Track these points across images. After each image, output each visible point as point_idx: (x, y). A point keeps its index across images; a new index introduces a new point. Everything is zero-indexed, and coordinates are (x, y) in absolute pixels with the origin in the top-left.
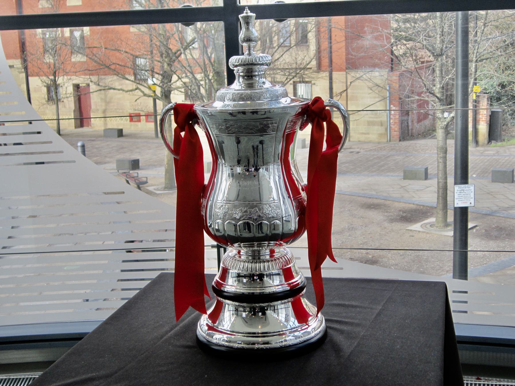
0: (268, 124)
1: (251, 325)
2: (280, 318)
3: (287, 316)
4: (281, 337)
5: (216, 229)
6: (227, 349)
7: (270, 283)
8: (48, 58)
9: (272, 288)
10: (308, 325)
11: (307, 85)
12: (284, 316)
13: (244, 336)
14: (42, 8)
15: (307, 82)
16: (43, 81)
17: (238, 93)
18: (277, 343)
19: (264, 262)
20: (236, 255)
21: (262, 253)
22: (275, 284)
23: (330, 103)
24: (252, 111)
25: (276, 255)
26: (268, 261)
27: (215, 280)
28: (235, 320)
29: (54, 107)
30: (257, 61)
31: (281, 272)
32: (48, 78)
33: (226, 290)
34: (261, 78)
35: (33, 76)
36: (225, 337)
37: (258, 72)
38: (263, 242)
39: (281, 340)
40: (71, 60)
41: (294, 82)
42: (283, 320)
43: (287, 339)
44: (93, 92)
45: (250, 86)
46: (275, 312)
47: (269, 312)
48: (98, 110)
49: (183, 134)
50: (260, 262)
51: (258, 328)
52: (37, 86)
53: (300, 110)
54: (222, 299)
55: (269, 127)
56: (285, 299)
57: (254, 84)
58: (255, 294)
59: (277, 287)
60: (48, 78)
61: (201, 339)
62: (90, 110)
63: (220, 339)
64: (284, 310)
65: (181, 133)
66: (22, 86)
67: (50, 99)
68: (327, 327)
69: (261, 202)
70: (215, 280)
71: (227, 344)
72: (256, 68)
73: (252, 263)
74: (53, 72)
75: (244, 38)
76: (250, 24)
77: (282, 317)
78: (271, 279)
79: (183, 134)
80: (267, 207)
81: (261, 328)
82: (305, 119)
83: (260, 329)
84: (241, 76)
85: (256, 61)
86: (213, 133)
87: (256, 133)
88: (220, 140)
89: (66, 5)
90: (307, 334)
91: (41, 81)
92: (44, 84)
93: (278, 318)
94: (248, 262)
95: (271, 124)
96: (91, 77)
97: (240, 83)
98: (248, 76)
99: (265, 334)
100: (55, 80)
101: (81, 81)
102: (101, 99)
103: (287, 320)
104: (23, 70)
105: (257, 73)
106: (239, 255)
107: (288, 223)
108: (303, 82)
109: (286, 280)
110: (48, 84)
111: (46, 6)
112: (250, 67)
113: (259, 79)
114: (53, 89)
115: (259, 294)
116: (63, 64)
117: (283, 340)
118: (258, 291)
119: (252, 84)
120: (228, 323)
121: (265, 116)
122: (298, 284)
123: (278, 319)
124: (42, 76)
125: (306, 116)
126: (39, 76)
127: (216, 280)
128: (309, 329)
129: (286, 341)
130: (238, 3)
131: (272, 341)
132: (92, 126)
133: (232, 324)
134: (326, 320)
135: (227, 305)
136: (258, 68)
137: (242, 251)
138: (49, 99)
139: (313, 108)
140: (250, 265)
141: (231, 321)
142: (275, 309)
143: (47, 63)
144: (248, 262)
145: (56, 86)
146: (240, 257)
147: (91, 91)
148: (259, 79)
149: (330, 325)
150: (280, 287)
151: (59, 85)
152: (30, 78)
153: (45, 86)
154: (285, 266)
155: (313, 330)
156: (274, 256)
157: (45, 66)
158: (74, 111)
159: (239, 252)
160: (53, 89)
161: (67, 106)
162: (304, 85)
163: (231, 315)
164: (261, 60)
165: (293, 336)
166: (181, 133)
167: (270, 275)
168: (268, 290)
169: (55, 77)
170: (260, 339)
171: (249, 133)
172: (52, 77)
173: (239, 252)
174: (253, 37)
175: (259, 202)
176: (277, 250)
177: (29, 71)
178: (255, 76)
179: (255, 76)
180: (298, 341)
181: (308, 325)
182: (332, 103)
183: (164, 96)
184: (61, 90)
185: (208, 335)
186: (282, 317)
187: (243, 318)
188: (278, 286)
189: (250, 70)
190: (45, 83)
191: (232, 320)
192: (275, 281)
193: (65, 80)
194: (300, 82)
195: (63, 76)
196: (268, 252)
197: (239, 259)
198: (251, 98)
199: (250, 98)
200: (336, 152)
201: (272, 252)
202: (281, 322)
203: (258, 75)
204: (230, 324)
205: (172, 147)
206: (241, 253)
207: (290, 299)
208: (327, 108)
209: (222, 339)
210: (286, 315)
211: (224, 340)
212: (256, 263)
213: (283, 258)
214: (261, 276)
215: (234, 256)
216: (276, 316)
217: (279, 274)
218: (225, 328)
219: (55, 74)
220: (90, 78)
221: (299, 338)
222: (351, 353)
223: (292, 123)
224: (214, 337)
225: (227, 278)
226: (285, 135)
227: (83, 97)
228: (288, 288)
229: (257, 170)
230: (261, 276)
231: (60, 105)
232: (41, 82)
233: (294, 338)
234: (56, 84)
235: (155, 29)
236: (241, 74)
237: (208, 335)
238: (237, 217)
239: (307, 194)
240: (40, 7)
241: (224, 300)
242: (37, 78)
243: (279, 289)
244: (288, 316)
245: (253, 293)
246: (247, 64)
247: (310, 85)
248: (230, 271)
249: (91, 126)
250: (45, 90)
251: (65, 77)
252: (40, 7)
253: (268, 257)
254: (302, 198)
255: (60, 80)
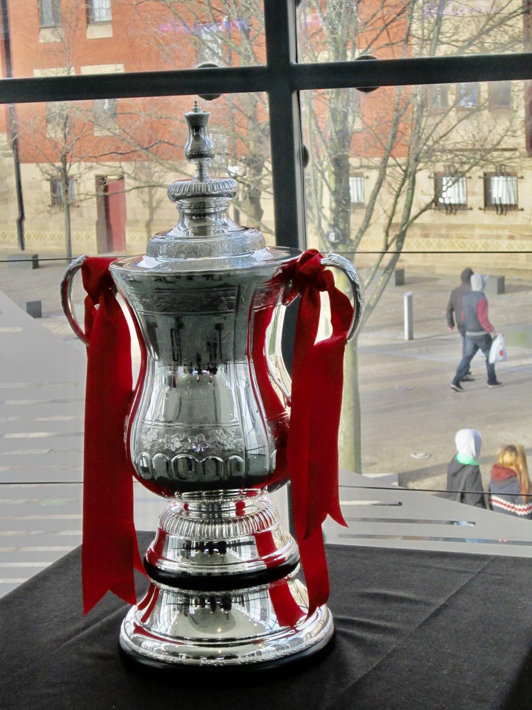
0: (220, 297)
1: (204, 628)
2: (252, 615)
3: (264, 611)
4: (256, 646)
5: (143, 468)
6: (163, 666)
7: (235, 558)
8: (53, 131)
9: (239, 566)
10: (294, 628)
11: (509, 179)
12: (258, 611)
13: (195, 645)
14: (44, 44)
15: (508, 175)
16: (43, 170)
17: (176, 244)
18: (245, 656)
19: (228, 522)
20: (182, 511)
21: (224, 507)
22: (244, 559)
23: (330, 260)
24: (204, 274)
25: (247, 511)
26: (235, 521)
27: (148, 549)
28: (177, 620)
29: (62, 216)
30: (209, 190)
31: (253, 539)
32: (53, 165)
33: (163, 568)
34: (220, 218)
35: (27, 161)
36: (163, 646)
37: (215, 207)
38: (232, 490)
39: (252, 652)
40: (92, 134)
41: (485, 174)
42: (258, 618)
43: (263, 650)
44: (131, 190)
45: (202, 232)
46: (243, 605)
47: (236, 607)
48: (137, 221)
49: (97, 306)
50: (222, 523)
51: (216, 632)
52: (34, 179)
53: (280, 271)
54: (155, 582)
55: (222, 302)
56: (259, 584)
57: (208, 229)
58: (212, 575)
59: (247, 565)
60: (53, 165)
61: (124, 646)
62: (124, 222)
63: (153, 649)
64: (258, 602)
65: (95, 306)
66: (8, 179)
67: (56, 202)
68: (336, 633)
69: (219, 425)
70: (148, 549)
71: (161, 657)
72: (212, 201)
73: (208, 524)
74: (61, 155)
75: (191, 151)
76: (202, 129)
77: (255, 613)
78: (236, 551)
79: (97, 306)
80: (220, 434)
81: (221, 632)
82: (290, 285)
83: (220, 634)
84: (186, 214)
85: (207, 190)
86: (139, 309)
87: (200, 311)
88: (152, 320)
89: (86, 37)
90: (297, 642)
91: (41, 170)
92: (46, 176)
93: (248, 615)
94: (196, 522)
95: (224, 296)
96: (123, 164)
97: (185, 226)
98: (200, 215)
99: (229, 642)
100: (65, 169)
101: (105, 171)
102: (144, 202)
103: (264, 617)
104: (11, 151)
105: (212, 211)
106: (186, 512)
107: (263, 457)
108: (502, 174)
109: (261, 554)
110: (52, 177)
111: (52, 41)
112: (201, 199)
113: (216, 220)
114: (60, 184)
115: (221, 575)
116: (78, 142)
117: (255, 652)
118: (217, 571)
119: (205, 227)
120: (167, 624)
121: (221, 283)
122: (283, 560)
123: (249, 617)
124: (43, 162)
125: (291, 281)
126: (37, 163)
127: (150, 549)
128: (301, 635)
129: (260, 653)
130: (293, 61)
131: (237, 652)
132: (128, 249)
133: (173, 627)
134: (336, 621)
135: (165, 594)
136: (215, 202)
137: (190, 505)
138: (54, 203)
139: (301, 269)
140: (198, 527)
141: (171, 621)
142: (243, 601)
143: (51, 140)
144: (196, 522)
145: (67, 180)
146: (188, 514)
147: (127, 188)
148: (216, 220)
149: (341, 629)
150: (252, 564)
151: (72, 176)
152: (22, 166)
153: (48, 180)
154: (264, 528)
155: (309, 636)
156: (244, 512)
157: (49, 144)
158: (98, 223)
159: (186, 506)
160: (60, 184)
161: (85, 214)
162: (504, 179)
163: (172, 611)
164: (215, 188)
165: (274, 646)
166: (95, 306)
167: (236, 545)
168: (232, 570)
169: (65, 164)
170: (220, 650)
171: (189, 311)
172: (59, 164)
173: (186, 506)
174: (205, 149)
175: (214, 425)
176: (248, 502)
177: (21, 153)
178: (210, 214)
179: (210, 214)
180: (281, 653)
181: (294, 628)
182: (334, 261)
183: (248, 199)
184: (75, 188)
185: (135, 641)
186: (255, 613)
187: (191, 616)
188: (249, 562)
189: (202, 205)
190: (48, 174)
191: (173, 620)
192: (243, 554)
193: (82, 169)
194: (496, 174)
195: (79, 161)
196: (232, 505)
197: (186, 518)
198: (196, 253)
199: (194, 252)
200: (344, 341)
201: (240, 506)
202: (253, 622)
203: (215, 213)
204: (170, 627)
205: (82, 327)
206: (189, 508)
207: (268, 585)
208: (327, 268)
209: (155, 649)
210: (261, 610)
211: (159, 651)
212: (215, 523)
213: (256, 517)
214: (222, 547)
215: (180, 514)
216: (246, 611)
217: (250, 543)
218: (163, 631)
219: (64, 161)
220: (121, 167)
221: (283, 648)
222: (364, 677)
223: (263, 294)
224: (143, 645)
225: (164, 549)
226: (253, 316)
227: (111, 201)
228: (265, 567)
229: (214, 371)
230: (222, 547)
231: (74, 214)
232: (40, 173)
233: (275, 649)
234: (66, 176)
235: (311, 59)
236: (188, 211)
237: (135, 641)
238: (172, 449)
239: (292, 411)
240: (41, 41)
241: (158, 584)
242: (34, 165)
243: (247, 568)
244: (265, 610)
245: (200, 574)
246: (198, 196)
247: (515, 178)
248: (171, 537)
249: (125, 249)
250: (47, 186)
251: (83, 164)
252: (41, 41)
253: (233, 514)
254: (284, 419)
255: (73, 170)
